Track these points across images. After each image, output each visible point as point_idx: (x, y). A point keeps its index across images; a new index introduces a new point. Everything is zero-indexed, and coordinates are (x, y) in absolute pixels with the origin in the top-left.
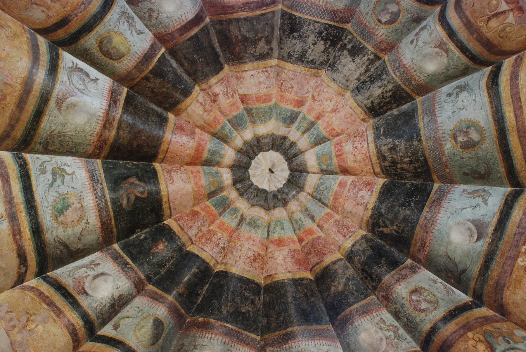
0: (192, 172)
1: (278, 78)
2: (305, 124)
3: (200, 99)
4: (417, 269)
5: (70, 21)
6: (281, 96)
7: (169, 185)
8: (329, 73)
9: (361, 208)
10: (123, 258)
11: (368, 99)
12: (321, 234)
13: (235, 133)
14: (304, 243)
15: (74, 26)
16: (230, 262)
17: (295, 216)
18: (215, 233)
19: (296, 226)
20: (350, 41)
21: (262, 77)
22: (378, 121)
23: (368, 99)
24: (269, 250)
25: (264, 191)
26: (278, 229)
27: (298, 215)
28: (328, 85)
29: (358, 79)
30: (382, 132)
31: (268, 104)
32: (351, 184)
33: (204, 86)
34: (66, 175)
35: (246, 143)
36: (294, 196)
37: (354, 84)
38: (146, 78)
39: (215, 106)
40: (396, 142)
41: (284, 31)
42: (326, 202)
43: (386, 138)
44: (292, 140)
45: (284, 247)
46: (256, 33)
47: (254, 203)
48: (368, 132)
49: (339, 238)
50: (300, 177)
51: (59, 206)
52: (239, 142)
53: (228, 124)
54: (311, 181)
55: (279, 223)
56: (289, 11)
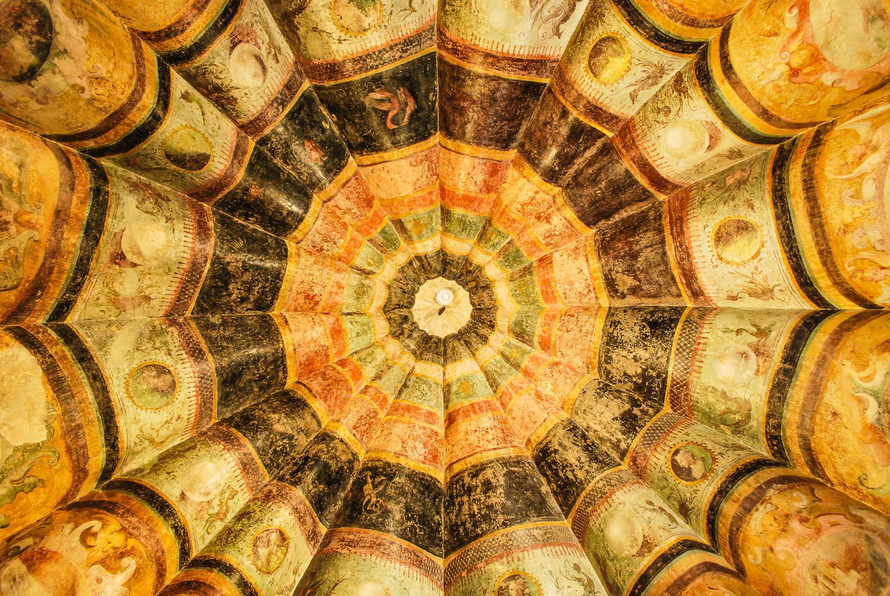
2: (515, 355)
8: (595, 385)
9: (399, 448)
10: (292, 98)
12: (355, 394)
14: (339, 368)
17: (378, 351)
19: (363, 354)
24: (324, 318)
27: (380, 355)
32: (432, 430)
33: (560, 200)
35: (480, 269)
41: (652, 313)
42: (403, 396)
49: (351, 419)
50: (437, 354)
52: (480, 258)
54: (430, 370)
55: (366, 329)
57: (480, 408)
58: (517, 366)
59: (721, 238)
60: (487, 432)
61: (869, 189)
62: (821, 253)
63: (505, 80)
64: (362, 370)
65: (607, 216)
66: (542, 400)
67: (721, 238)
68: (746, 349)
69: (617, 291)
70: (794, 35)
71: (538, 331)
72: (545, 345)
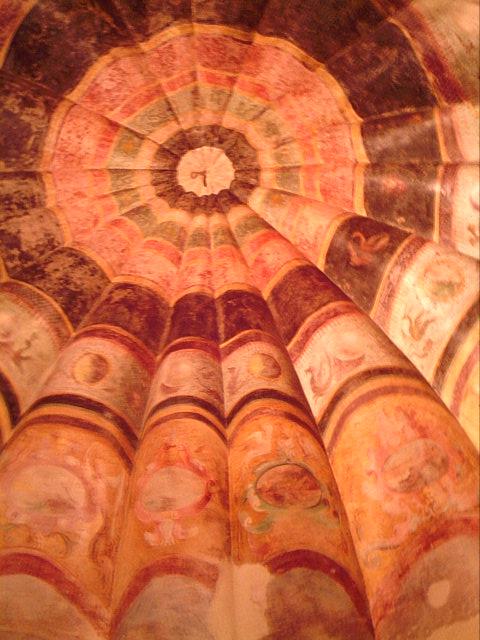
0: (291, 228)
1: (123, 261)
2: (126, 197)
3: (222, 281)
4: (103, 136)
5: (286, 413)
6: (131, 238)
7: (324, 227)
8: (58, 238)
9: (122, 65)
10: (440, 210)
11: (26, 183)
12: (199, 68)
13: (211, 231)
14: (231, 75)
15: (286, 407)
16: (335, 108)
17: (216, 107)
18: (323, 151)
19: (223, 97)
20: (11, 258)
21: (140, 267)
22: (31, 164)
23: (26, 183)
24: (279, 92)
25: (228, 154)
26: (248, 107)
27: (210, 105)
28: (68, 222)
29: (27, 214)
30: (32, 138)
31: (154, 238)
32: (117, 106)
33: (209, 291)
34: (413, 320)
35: (208, 215)
36: (198, 129)
37: (35, 212)
38: (258, 327)
39: (211, 268)
40: (17, 110)
41: (84, 303)
42: (164, 102)
43: (29, 125)
44: (153, 188)
45: (257, 82)
46: (115, 309)
47: (251, 150)
48: (52, 151)
49: (179, 47)
50: (174, 146)
51: (446, 292)
52: (216, 220)
53: (212, 244)
54: (163, 135)
55: (240, 112)
56: (65, 318)
57: (102, 146)
58: (115, 194)
59: (100, 361)
60: (79, 137)
61: (72, 461)
62: (49, 416)
63: (311, 313)
64: (213, 85)
65: (174, 317)
66: (75, 194)
67: (100, 361)
68: (12, 339)
69: (117, 289)
70: (188, 458)
71: (130, 222)
72: (116, 223)
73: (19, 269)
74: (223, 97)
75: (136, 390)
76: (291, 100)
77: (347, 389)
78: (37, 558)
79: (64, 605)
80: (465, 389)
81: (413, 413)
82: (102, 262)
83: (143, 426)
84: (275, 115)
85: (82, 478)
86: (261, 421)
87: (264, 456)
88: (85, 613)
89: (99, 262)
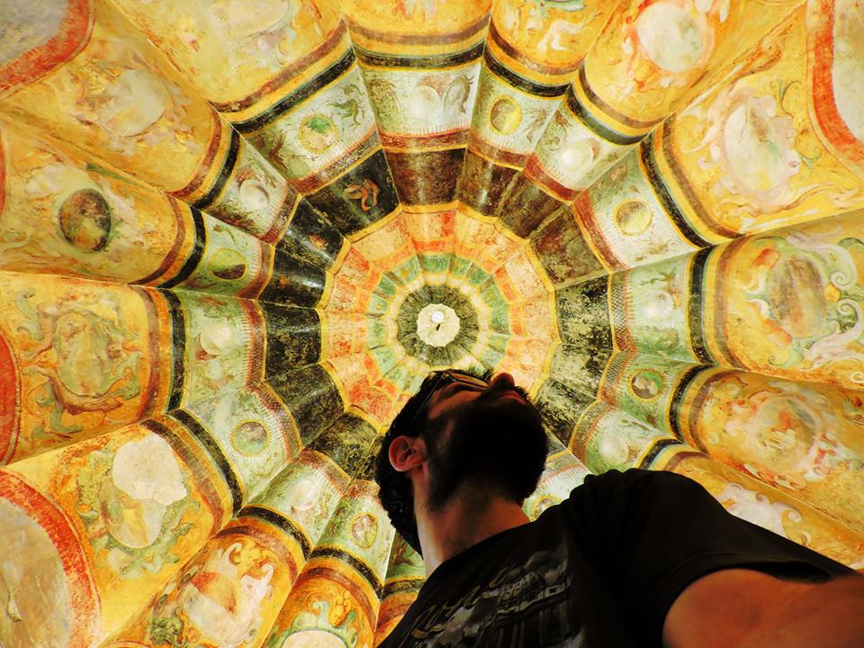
2: (499, 344)
11: (549, 398)
14: (377, 388)
17: (402, 368)
19: (392, 374)
24: (358, 356)
27: (404, 371)
31: (505, 298)
33: (499, 226)
35: (456, 290)
41: (587, 286)
59: (621, 218)
61: (716, 153)
62: (695, 208)
65: (535, 227)
67: (621, 218)
68: (661, 292)
70: (633, 57)
72: (518, 331)
73: (602, 350)
74: (392, 374)
75: (611, 181)
76: (354, 344)
77: (445, 60)
78: (817, 112)
79: (841, 45)
80: (329, 38)
81: (395, 12)
82: (552, 305)
83: (628, 152)
84: (369, 339)
85: (722, 130)
86: (544, 58)
87: (564, 18)
88: (831, 17)
89: (554, 305)
